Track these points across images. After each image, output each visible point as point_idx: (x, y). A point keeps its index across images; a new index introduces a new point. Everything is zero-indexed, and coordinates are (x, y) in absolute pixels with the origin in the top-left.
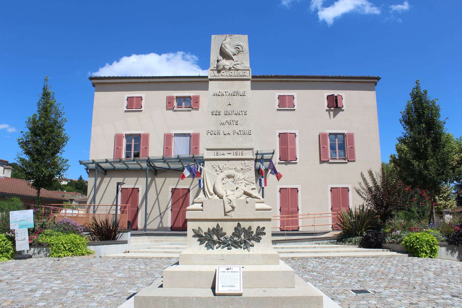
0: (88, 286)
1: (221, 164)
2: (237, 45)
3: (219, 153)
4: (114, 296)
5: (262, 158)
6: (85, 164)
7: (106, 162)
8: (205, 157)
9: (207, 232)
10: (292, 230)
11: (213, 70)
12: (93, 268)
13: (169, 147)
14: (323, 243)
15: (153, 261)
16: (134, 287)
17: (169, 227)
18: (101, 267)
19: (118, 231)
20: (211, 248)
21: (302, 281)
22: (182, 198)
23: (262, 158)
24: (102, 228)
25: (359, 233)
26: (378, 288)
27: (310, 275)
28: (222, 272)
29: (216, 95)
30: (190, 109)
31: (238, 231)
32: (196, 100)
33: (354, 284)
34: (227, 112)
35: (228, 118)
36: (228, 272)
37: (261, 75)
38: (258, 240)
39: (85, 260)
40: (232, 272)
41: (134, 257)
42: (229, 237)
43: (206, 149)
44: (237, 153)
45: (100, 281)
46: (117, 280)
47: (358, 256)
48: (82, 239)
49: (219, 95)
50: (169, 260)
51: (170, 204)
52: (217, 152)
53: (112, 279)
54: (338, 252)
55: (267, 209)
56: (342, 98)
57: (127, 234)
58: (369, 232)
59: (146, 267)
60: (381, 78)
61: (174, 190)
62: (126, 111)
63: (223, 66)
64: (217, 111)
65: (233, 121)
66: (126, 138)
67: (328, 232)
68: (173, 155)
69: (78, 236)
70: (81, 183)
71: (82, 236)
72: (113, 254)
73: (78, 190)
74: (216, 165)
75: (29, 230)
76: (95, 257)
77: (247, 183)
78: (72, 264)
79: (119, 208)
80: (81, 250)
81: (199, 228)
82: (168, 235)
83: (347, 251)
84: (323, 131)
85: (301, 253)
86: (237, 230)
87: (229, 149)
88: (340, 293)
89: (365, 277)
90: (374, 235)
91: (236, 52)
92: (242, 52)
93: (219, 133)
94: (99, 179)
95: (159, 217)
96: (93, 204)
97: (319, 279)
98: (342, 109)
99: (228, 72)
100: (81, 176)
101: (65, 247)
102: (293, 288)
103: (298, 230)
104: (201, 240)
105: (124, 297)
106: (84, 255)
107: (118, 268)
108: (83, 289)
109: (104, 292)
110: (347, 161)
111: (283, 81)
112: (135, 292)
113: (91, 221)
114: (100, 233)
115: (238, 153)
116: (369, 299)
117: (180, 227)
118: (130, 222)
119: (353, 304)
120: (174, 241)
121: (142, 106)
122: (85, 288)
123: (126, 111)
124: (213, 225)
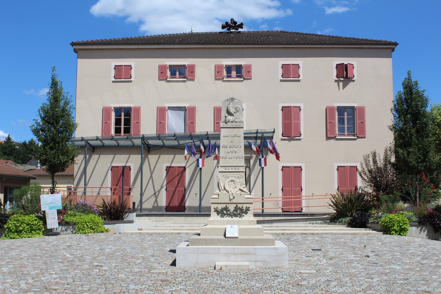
1: (228, 174)
10: (295, 212)
13: (163, 122)
14: (316, 223)
17: (164, 207)
22: (177, 177)
25: (349, 214)
30: (185, 79)
32: (192, 68)
35: (231, 150)
42: (232, 212)
47: (339, 233)
49: (226, 137)
51: (165, 183)
56: (354, 67)
57: (133, 215)
60: (398, 44)
61: (168, 169)
62: (114, 81)
70: (9, 146)
72: (129, 231)
75: (58, 210)
82: (168, 215)
83: (333, 229)
95: (153, 197)
98: (353, 79)
101: (87, 225)
103: (301, 212)
106: (103, 232)
110: (356, 138)
111: (288, 48)
117: (175, 206)
124: (224, 206)
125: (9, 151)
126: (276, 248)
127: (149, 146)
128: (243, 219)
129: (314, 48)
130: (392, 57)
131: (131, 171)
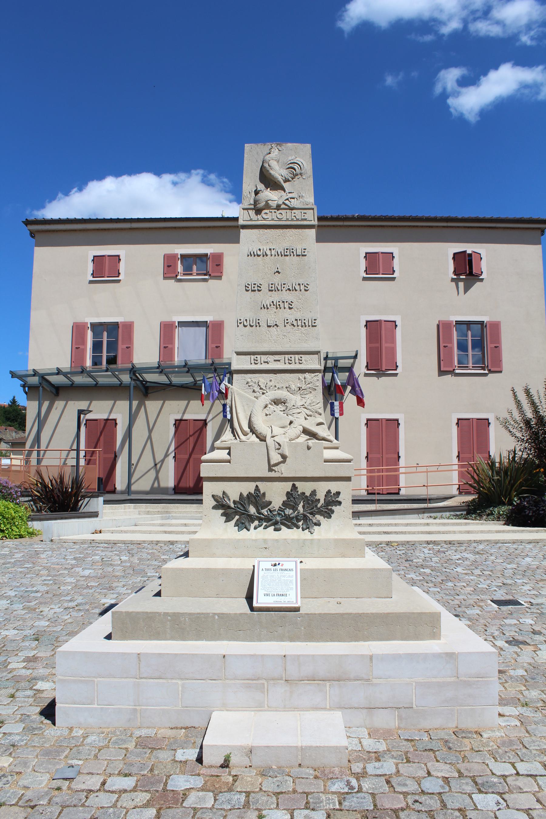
0: (32, 592)
1: (263, 379)
2: (291, 163)
3: (259, 359)
4: (76, 608)
5: (336, 366)
6: (20, 377)
7: (58, 374)
8: (234, 367)
9: (238, 500)
11: (247, 209)
12: (40, 560)
13: (170, 346)
14: (442, 517)
15: (144, 548)
16: (110, 593)
17: (171, 488)
18: (53, 558)
19: (81, 494)
20: (246, 528)
21: (403, 584)
22: (192, 437)
23: (336, 366)
24: (52, 490)
25: (506, 500)
26: (536, 596)
27: (419, 574)
28: (264, 570)
29: (253, 255)
30: (207, 277)
31: (292, 499)
32: (218, 259)
33: (496, 589)
34: (273, 286)
35: (276, 297)
36: (275, 570)
37: (335, 215)
38: (329, 513)
39: (25, 546)
40: (282, 570)
41: (109, 540)
42: (277, 508)
43: (235, 352)
44: (291, 361)
45: (51, 582)
46: (82, 581)
48: (19, 509)
49: (258, 256)
50: (171, 546)
51: (172, 448)
52: (256, 359)
53: (72, 580)
54: (468, 532)
55: (343, 459)
56: (481, 258)
57: (98, 501)
58: (524, 498)
59: (132, 559)
61: (178, 423)
63: (267, 202)
64: (255, 284)
65: (283, 302)
66: (93, 330)
67: (451, 498)
68: (176, 359)
69: (11, 504)
70: (14, 410)
71: (18, 504)
73: (9, 423)
74: (254, 381)
76: (42, 541)
77: (309, 413)
78: (2, 552)
79: (82, 454)
80: (18, 528)
81: (224, 493)
83: (484, 531)
84: (444, 318)
85: (403, 534)
86: (290, 496)
87: (276, 352)
88: (470, 605)
89: (514, 577)
90: (533, 503)
91: (289, 176)
92: (299, 176)
93: (259, 323)
94: (46, 404)
96: (36, 448)
97: (435, 580)
98: (481, 277)
99: (275, 212)
100: (14, 397)
102: (388, 599)
103: (398, 494)
104: (227, 513)
105: (94, 611)
106: (23, 537)
107: (83, 560)
108: (24, 597)
109: (59, 603)
110: (486, 372)
112: (113, 602)
113: (33, 478)
114: (50, 498)
115: (293, 359)
116: (521, 616)
117: (189, 486)
118: (102, 479)
119: (492, 625)
120: (180, 512)
121: (120, 272)
122: (26, 594)
123: (91, 282)
124: (248, 488)
125: (14, 417)
126: (451, 656)
127: (148, 384)
128: (316, 536)
129: (417, 226)
130: (542, 243)
131: (118, 427)
